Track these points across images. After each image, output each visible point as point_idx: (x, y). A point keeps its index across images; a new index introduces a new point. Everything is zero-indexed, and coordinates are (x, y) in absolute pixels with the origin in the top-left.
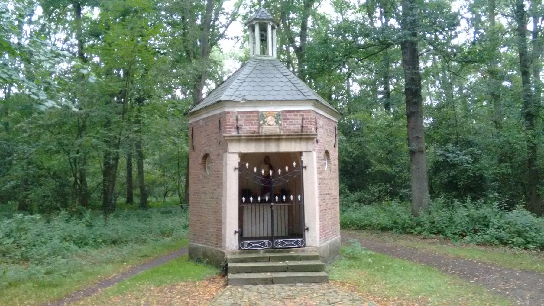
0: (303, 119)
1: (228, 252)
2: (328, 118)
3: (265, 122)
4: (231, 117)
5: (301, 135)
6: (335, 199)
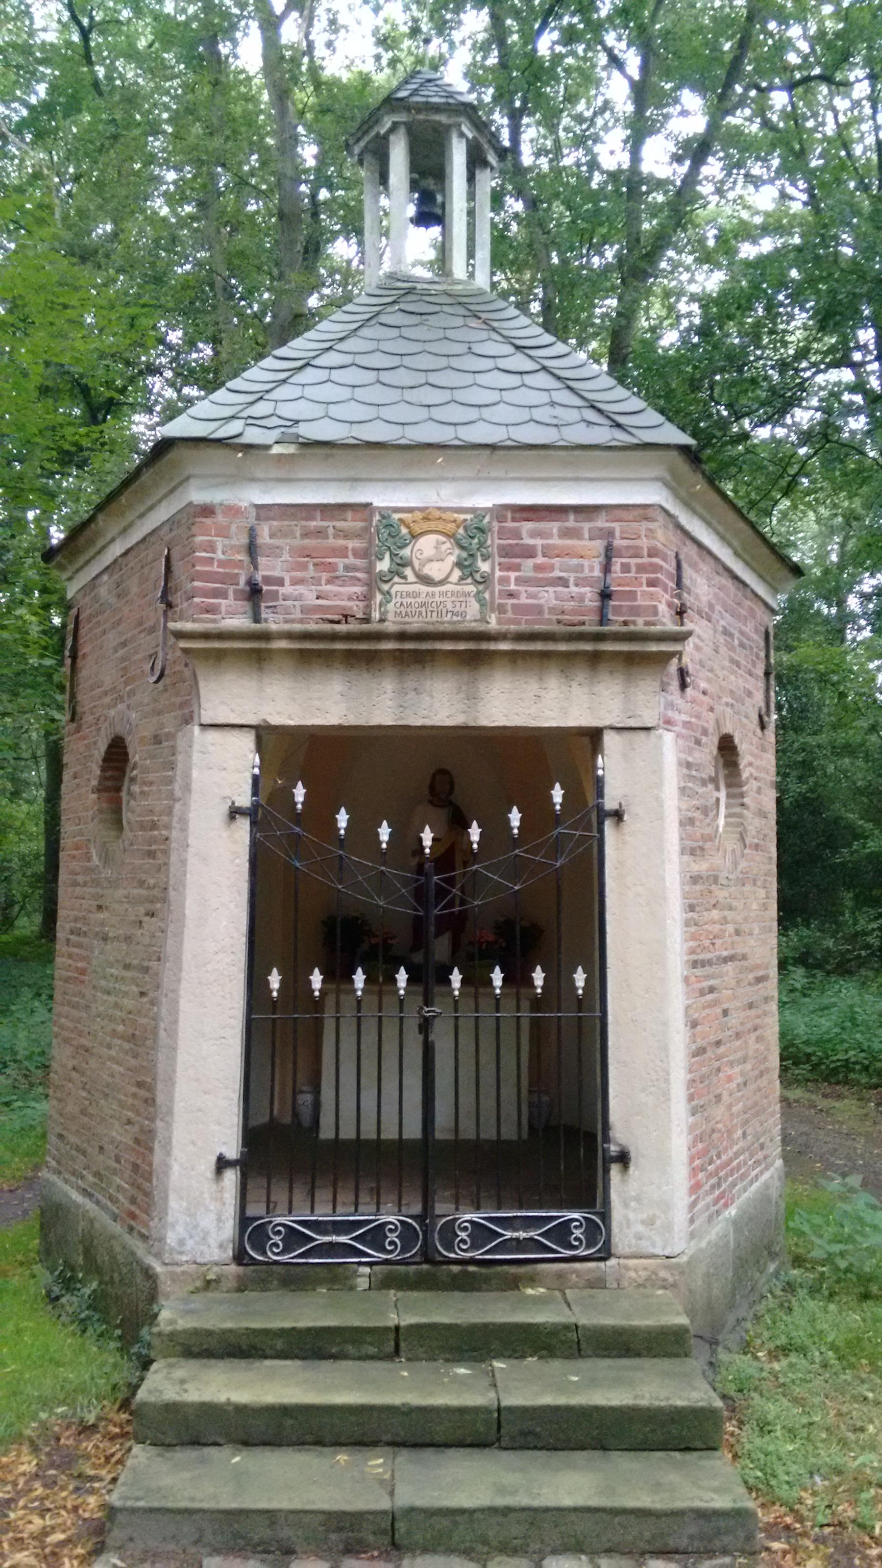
0: (609, 553)
1: (174, 1277)
2: (736, 578)
3: (405, 563)
4: (223, 532)
5: (599, 637)
6: (759, 980)
